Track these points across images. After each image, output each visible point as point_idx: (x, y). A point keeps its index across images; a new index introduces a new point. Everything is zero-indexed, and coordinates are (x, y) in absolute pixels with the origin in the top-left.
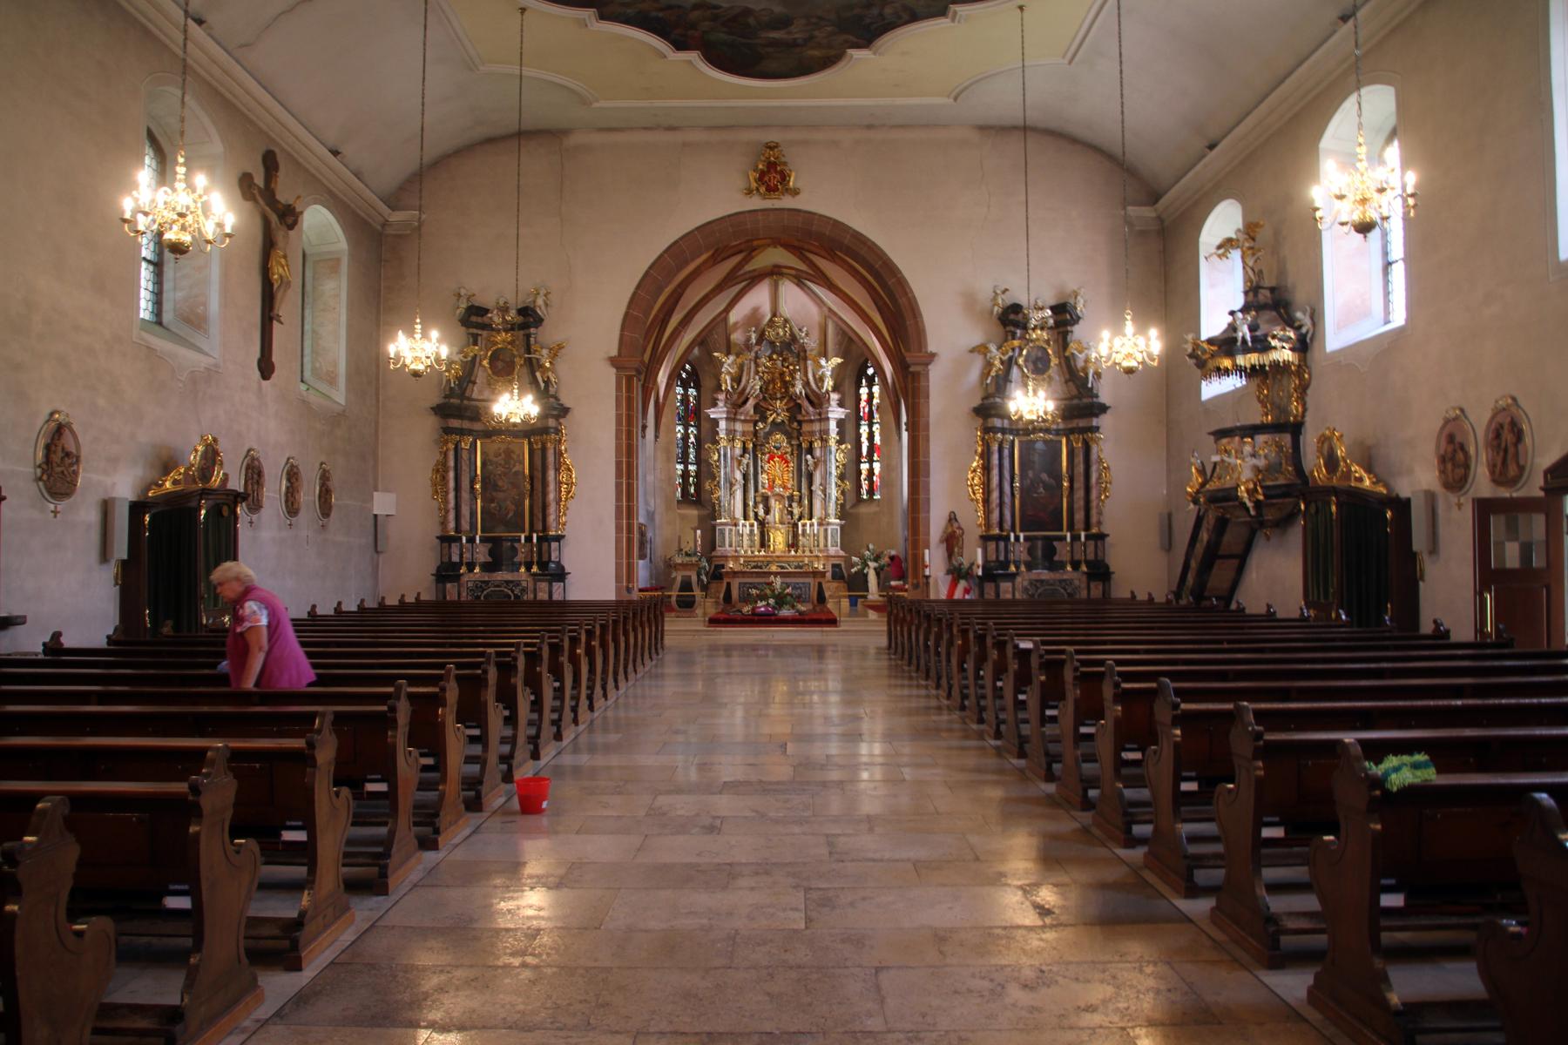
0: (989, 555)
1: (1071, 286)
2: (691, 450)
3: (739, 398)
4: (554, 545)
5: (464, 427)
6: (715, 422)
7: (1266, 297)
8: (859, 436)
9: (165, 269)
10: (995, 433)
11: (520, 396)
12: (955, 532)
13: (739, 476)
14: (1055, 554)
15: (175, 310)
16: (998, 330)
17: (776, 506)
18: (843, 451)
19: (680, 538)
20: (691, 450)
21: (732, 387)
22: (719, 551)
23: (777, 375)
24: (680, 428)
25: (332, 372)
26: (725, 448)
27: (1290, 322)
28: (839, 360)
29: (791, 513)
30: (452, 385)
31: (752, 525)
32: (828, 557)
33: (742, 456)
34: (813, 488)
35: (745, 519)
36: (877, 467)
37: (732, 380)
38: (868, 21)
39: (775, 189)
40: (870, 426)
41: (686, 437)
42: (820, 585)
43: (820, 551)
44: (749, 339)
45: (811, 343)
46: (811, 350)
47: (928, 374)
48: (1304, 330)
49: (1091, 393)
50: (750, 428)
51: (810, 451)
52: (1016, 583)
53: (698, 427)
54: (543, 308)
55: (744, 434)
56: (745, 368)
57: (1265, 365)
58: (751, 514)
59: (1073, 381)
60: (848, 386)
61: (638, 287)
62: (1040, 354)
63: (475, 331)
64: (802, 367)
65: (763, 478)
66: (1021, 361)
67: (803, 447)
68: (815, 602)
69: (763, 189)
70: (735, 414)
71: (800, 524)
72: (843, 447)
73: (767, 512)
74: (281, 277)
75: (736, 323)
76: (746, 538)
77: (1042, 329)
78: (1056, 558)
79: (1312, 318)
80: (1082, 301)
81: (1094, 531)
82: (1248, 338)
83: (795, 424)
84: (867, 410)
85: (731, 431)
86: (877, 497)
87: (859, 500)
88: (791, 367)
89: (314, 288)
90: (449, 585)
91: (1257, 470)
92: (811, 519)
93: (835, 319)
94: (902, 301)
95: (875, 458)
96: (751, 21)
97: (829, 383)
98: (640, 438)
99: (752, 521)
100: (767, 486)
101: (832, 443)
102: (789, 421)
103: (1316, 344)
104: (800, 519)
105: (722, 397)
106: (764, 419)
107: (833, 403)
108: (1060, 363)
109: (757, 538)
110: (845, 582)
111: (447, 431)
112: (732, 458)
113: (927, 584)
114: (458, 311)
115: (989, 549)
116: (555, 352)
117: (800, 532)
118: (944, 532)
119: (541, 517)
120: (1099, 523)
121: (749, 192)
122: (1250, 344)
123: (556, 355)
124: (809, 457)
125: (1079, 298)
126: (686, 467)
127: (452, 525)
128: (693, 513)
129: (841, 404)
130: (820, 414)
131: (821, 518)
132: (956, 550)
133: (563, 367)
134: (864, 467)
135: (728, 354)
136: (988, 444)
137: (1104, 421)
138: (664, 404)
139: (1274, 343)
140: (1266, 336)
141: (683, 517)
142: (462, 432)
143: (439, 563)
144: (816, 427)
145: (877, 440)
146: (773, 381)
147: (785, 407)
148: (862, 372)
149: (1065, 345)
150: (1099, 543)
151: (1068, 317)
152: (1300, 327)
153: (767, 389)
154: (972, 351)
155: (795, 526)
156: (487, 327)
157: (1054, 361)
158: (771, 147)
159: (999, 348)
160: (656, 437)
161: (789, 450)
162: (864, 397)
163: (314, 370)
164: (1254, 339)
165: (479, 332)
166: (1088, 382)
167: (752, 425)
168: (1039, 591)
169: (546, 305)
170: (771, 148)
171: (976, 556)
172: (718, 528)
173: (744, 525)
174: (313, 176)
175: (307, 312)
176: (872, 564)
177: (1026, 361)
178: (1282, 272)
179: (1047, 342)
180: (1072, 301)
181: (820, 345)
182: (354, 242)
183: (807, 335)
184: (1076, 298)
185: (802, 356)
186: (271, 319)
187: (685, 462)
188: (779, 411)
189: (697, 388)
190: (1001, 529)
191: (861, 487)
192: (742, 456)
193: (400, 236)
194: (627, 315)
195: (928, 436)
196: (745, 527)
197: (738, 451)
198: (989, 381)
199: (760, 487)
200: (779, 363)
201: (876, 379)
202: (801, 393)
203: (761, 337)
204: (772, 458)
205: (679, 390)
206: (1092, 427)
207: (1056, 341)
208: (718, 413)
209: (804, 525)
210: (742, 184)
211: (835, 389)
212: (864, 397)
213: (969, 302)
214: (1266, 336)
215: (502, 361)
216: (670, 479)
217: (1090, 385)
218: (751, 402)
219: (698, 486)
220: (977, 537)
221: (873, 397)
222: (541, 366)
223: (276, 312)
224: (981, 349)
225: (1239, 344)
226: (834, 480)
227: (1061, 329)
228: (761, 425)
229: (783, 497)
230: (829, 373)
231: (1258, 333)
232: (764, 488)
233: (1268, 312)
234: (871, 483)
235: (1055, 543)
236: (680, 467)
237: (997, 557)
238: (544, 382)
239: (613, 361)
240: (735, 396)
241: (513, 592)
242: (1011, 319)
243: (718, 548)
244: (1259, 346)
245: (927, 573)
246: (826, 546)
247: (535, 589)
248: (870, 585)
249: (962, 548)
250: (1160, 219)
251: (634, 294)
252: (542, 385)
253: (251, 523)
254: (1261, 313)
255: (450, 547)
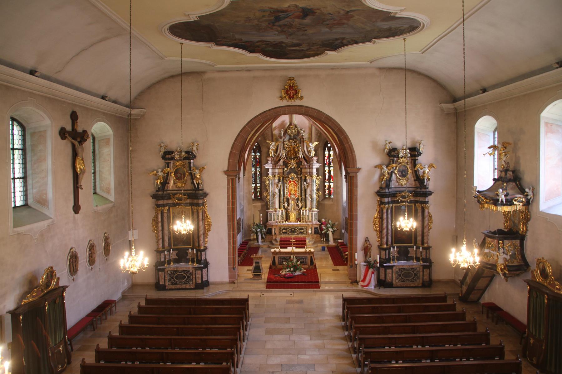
0: (382, 256)
1: (418, 138)
2: (258, 178)
3: (277, 159)
4: (203, 253)
5: (165, 203)
6: (268, 170)
7: (510, 175)
8: (325, 171)
9: (28, 179)
10: (385, 205)
11: (408, 218)
12: (368, 246)
13: (277, 191)
14: (409, 253)
15: (33, 198)
16: (386, 159)
17: (292, 202)
18: (318, 179)
19: (254, 215)
20: (258, 178)
21: (274, 155)
22: (270, 222)
23: (292, 149)
24: (253, 169)
25: (109, 188)
26: (271, 180)
27: (522, 191)
28: (317, 143)
29: (298, 205)
30: (159, 187)
31: (282, 211)
32: (313, 225)
33: (278, 183)
34: (307, 196)
35: (280, 208)
36: (332, 184)
37: (274, 152)
38: (335, 44)
39: (293, 97)
40: (329, 167)
41: (256, 173)
42: (311, 257)
43: (310, 222)
44: (280, 134)
45: (306, 135)
46: (305, 138)
47: (357, 177)
48: (529, 197)
49: (426, 187)
50: (281, 171)
51: (305, 180)
52: (393, 269)
53: (260, 168)
54: (196, 151)
55: (279, 173)
56: (279, 146)
57: (510, 212)
58: (282, 206)
59: (418, 181)
60: (320, 152)
61: (236, 140)
62: (404, 168)
63: (168, 161)
64: (302, 145)
65: (286, 191)
66: (396, 172)
67: (303, 178)
68: (309, 264)
69: (287, 97)
70: (275, 166)
71: (301, 210)
72: (318, 178)
73: (288, 205)
74: (81, 170)
75: (275, 127)
76: (280, 217)
77: (405, 157)
78: (409, 255)
79: (533, 192)
80: (422, 147)
81: (426, 246)
82: (504, 201)
83: (299, 169)
84: (328, 161)
85: (274, 173)
86: (332, 197)
87: (325, 198)
88: (297, 145)
89: (99, 152)
90: (160, 273)
91: (505, 260)
92: (306, 208)
93: (316, 126)
94: (346, 145)
95: (331, 181)
96: (284, 45)
97: (313, 153)
98: (237, 182)
99: (282, 209)
100: (288, 194)
101: (314, 178)
102: (297, 167)
103: (534, 204)
104: (301, 208)
105: (270, 159)
106: (287, 167)
107: (315, 161)
108: (412, 172)
109: (284, 216)
110: (319, 235)
111: (158, 206)
112: (274, 184)
113: (356, 267)
114: (161, 153)
115: (382, 254)
116: (201, 170)
117: (302, 214)
118: (363, 246)
119: (197, 240)
120: (427, 243)
121: (282, 98)
122: (504, 203)
123: (202, 172)
124: (305, 183)
125: (421, 145)
126: (256, 185)
127: (161, 245)
128: (259, 204)
129: (318, 162)
130: (309, 166)
131: (310, 208)
132: (368, 254)
133: (205, 176)
134: (327, 184)
135: (272, 141)
136: (382, 209)
137: (430, 199)
138: (247, 162)
139: (515, 203)
140: (512, 199)
141: (255, 207)
142: (164, 206)
143: (156, 261)
144: (308, 170)
145: (332, 173)
146: (290, 151)
147: (295, 162)
148: (326, 145)
149: (415, 165)
150: (427, 251)
151: (416, 153)
152: (527, 195)
153: (288, 154)
154: (376, 167)
155: (299, 210)
156: (173, 158)
157: (410, 171)
158: (291, 79)
159: (387, 167)
160: (244, 176)
161: (297, 180)
162: (327, 155)
163: (100, 187)
164: (506, 200)
165: (170, 162)
166: (424, 183)
167: (282, 169)
168: (403, 273)
169: (197, 149)
170: (291, 80)
171: (376, 257)
172: (269, 213)
173: (279, 211)
174: (96, 111)
175: (97, 163)
176: (330, 229)
177: (398, 171)
178: (517, 162)
179: (407, 163)
180: (418, 145)
181: (309, 134)
182: (115, 130)
183: (304, 132)
184: (420, 145)
185: (302, 141)
186: (78, 188)
187: (255, 183)
188: (293, 164)
189: (260, 152)
190: (387, 245)
191: (326, 192)
192: (278, 183)
193: (136, 119)
194: (231, 152)
195: (357, 204)
196: (280, 213)
197: (277, 181)
198: (383, 183)
199: (285, 195)
200: (293, 143)
201: (332, 148)
202: (302, 157)
203: (285, 132)
204: (290, 182)
205: (253, 154)
206: (426, 202)
207: (411, 163)
208: (268, 166)
209: (303, 211)
210: (278, 95)
211: (315, 155)
212: (327, 155)
213: (375, 145)
214: (512, 199)
215: (180, 173)
216: (250, 192)
217: (425, 184)
218: (282, 161)
219: (261, 194)
220: (377, 246)
221: (330, 156)
222: (196, 177)
223: (79, 184)
224: (379, 166)
225: (500, 202)
226: (315, 191)
227: (413, 158)
228: (286, 169)
229: (295, 199)
230: (313, 149)
231: (508, 197)
232: (287, 195)
233: (511, 183)
234: (330, 191)
235: (409, 249)
236: (254, 185)
237: (385, 257)
238: (197, 184)
239: (226, 173)
240: (275, 158)
241: (186, 274)
242: (392, 153)
243: (269, 221)
244: (508, 204)
245: (356, 263)
246: (312, 220)
247: (196, 274)
248: (330, 238)
249: (371, 253)
250: (456, 109)
251: (234, 143)
252: (196, 185)
253: (73, 279)
254: (508, 183)
255: (160, 255)
